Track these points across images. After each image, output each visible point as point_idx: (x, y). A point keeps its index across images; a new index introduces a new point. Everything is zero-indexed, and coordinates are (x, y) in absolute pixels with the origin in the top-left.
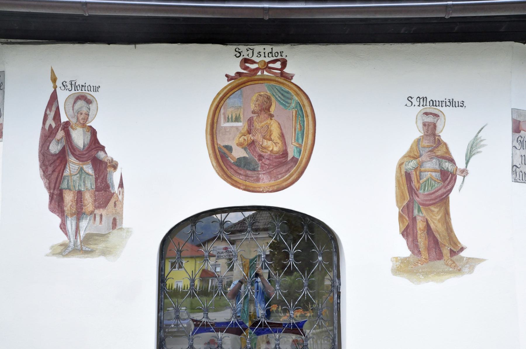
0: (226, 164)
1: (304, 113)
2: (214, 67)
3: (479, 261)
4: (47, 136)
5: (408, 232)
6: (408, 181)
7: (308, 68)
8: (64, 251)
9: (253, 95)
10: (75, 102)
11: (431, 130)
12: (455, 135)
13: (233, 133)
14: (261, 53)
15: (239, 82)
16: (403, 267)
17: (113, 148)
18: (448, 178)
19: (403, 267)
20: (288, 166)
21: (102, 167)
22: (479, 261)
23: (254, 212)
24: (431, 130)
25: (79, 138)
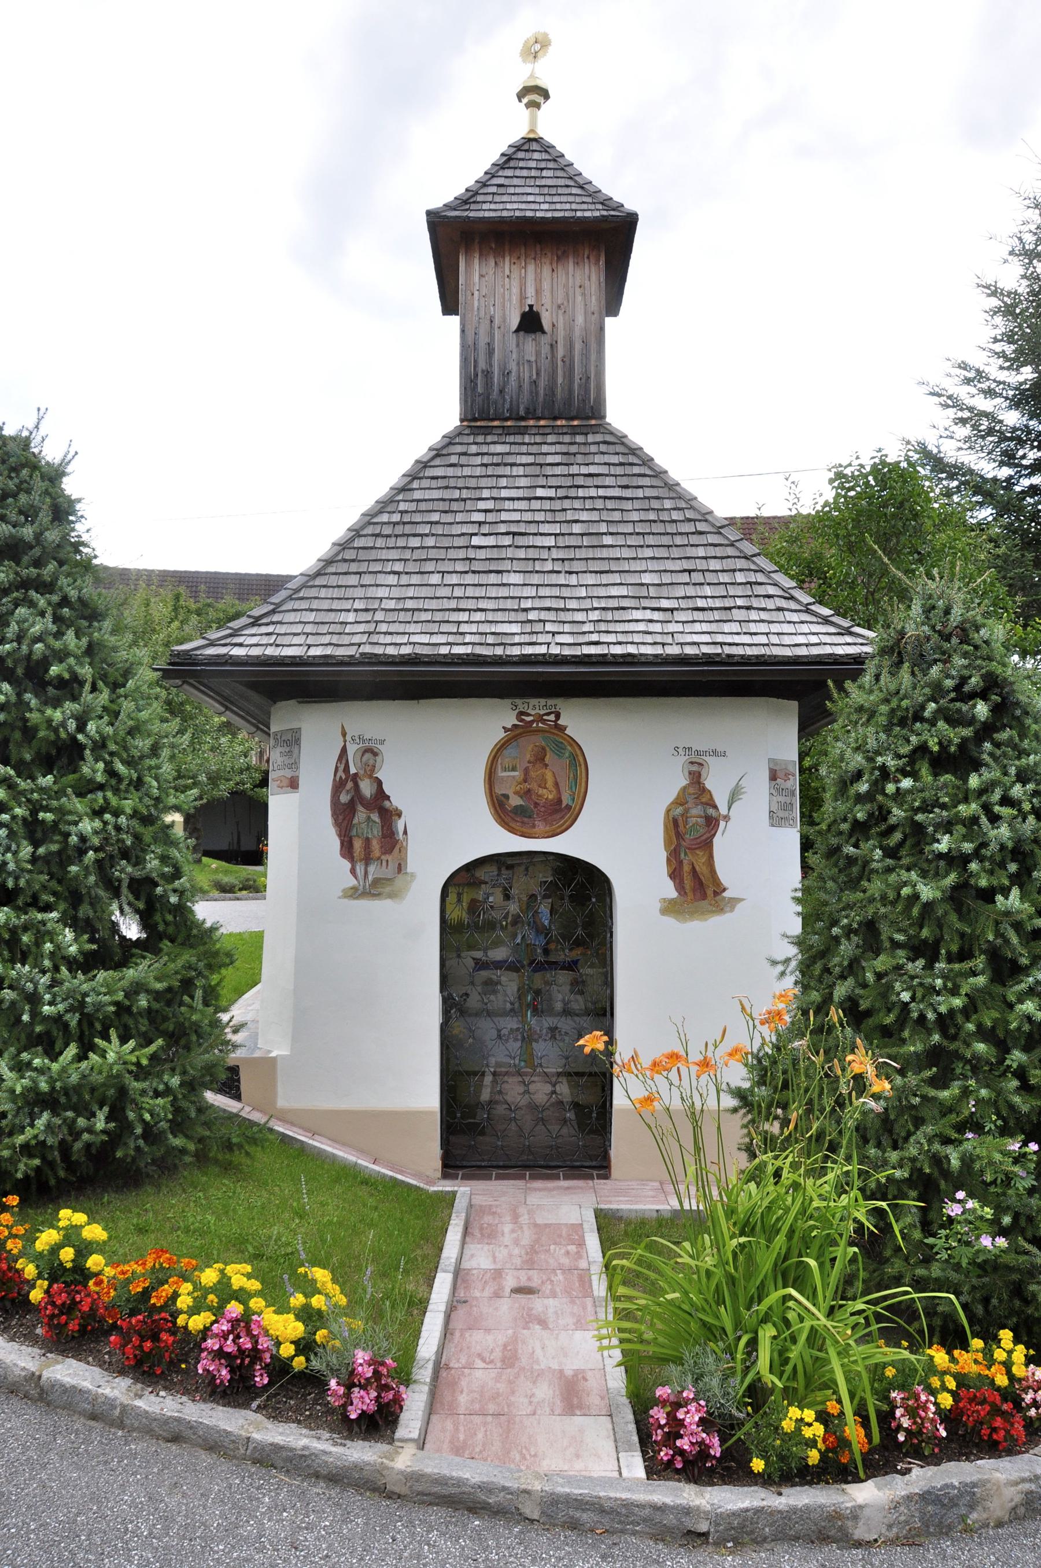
0: (506, 814)
2: (488, 724)
4: (338, 787)
7: (583, 723)
8: (354, 893)
9: (529, 746)
11: (696, 779)
13: (510, 780)
14: (536, 707)
15: (514, 735)
16: (670, 908)
17: (397, 800)
18: (712, 823)
19: (670, 908)
20: (562, 814)
21: (388, 815)
24: (696, 779)
25: (367, 788)
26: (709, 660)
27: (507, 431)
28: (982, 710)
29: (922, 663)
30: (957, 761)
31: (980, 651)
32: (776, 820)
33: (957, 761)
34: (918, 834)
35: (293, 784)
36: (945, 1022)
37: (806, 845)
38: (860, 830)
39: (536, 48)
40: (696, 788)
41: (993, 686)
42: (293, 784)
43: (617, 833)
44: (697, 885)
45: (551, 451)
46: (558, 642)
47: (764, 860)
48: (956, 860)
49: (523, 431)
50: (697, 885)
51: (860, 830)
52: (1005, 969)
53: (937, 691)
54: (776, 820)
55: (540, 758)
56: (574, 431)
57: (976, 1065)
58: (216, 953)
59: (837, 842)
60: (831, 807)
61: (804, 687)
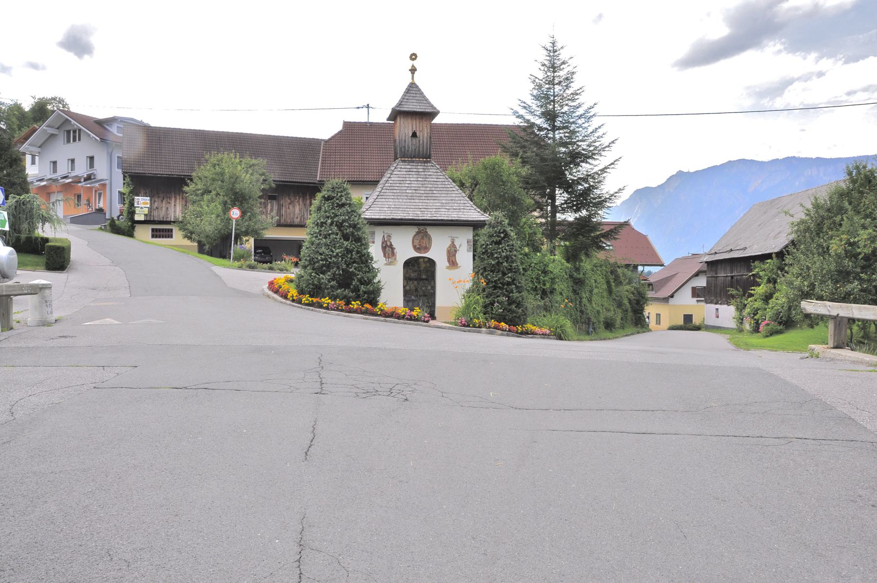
0: (417, 249)
1: (430, 239)
2: (413, 231)
3: (553, 51)
4: (383, 243)
5: (449, 261)
6: (449, 252)
7: (431, 231)
8: (386, 264)
9: (421, 235)
10: (697, 275)
11: (453, 242)
12: (457, 244)
13: (417, 242)
14: (422, 228)
15: (418, 233)
16: (448, 268)
17: (394, 246)
18: (456, 251)
19: (448, 268)
20: (427, 249)
21: (393, 249)
22: (553, 51)
23: (116, 322)
24: (453, 242)
25: (388, 244)
26: (457, 220)
27: (410, 162)
28: (502, 235)
29: (494, 228)
30: (498, 243)
31: (503, 226)
32: (468, 251)
33: (498, 243)
34: (492, 254)
35: (373, 242)
36: (495, 281)
37: (474, 256)
38: (484, 253)
39: (413, 57)
40: (453, 244)
41: (504, 231)
42: (373, 242)
43: (437, 252)
44: (453, 263)
45: (420, 168)
46: (428, 216)
47: (465, 258)
48: (497, 258)
49: (413, 162)
50: (453, 263)
51: (484, 253)
52: (504, 274)
53: (496, 232)
54: (468, 251)
55: (422, 238)
56: (425, 162)
57: (500, 288)
58: (854, 181)
59: (479, 254)
60: (479, 250)
61: (476, 225)
